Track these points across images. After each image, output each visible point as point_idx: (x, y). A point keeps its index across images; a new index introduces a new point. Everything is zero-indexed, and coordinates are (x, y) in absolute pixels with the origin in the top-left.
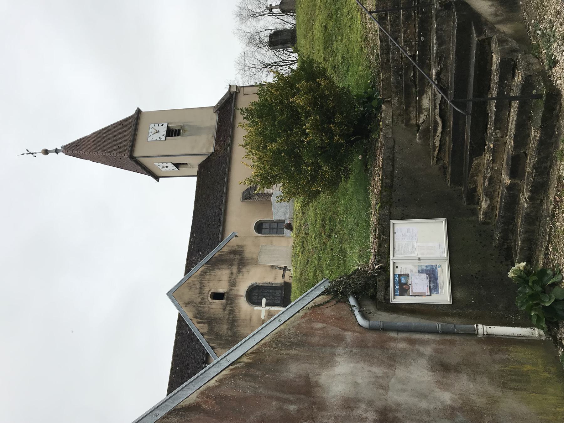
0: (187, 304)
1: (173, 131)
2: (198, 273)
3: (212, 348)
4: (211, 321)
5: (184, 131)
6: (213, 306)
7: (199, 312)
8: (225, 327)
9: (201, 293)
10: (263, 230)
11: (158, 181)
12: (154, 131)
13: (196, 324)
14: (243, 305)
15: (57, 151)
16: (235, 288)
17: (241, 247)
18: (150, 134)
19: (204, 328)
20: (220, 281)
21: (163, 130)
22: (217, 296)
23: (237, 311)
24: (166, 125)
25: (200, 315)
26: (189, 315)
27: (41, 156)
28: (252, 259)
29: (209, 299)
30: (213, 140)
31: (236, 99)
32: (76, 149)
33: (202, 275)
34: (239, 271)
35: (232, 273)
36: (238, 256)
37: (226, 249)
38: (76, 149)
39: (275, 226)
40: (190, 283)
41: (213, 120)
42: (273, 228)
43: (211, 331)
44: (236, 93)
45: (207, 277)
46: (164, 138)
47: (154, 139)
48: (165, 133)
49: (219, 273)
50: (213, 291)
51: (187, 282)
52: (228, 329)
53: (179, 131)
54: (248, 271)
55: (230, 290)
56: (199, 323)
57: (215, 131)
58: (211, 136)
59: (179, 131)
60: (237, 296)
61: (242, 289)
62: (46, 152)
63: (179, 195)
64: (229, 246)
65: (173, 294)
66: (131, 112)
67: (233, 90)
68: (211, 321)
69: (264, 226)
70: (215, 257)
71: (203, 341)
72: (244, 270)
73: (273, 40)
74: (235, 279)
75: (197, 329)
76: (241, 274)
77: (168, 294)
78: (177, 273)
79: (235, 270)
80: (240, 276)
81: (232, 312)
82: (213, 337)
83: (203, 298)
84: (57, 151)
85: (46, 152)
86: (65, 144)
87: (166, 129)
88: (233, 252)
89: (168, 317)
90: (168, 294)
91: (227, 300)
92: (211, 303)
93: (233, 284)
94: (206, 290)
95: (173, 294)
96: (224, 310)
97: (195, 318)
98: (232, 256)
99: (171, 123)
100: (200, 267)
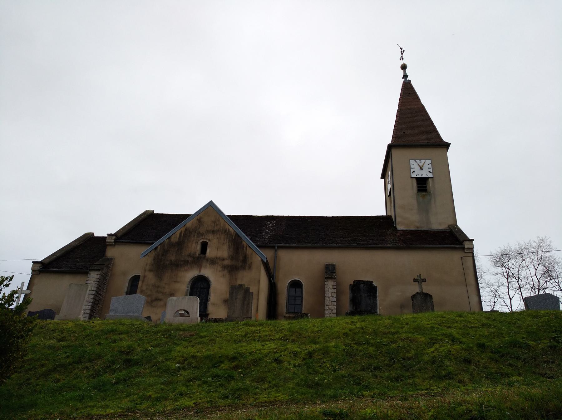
0: (199, 221)
1: (425, 184)
2: (227, 227)
3: (156, 248)
4: (180, 244)
5: (424, 196)
6: (194, 245)
7: (190, 233)
8: (173, 258)
9: (208, 232)
10: (294, 289)
11: (381, 178)
12: (421, 164)
13: (180, 231)
14: (190, 274)
15: (405, 76)
16: (208, 265)
17: (250, 267)
18: (418, 161)
19: (175, 239)
20: (218, 249)
21: (425, 173)
22: (204, 246)
23: (186, 268)
24: (430, 175)
25: (188, 233)
26: (189, 224)
27: (401, 63)
28: (236, 279)
29: (201, 241)
30: (412, 228)
31: (455, 249)
32: (408, 93)
33: (226, 231)
34: (225, 267)
35: (223, 260)
36: (240, 264)
37: (249, 251)
38: (408, 93)
39: (298, 302)
40: (219, 220)
41: (438, 224)
42: (295, 299)
43: (171, 245)
44: (463, 248)
45: (223, 236)
46: (414, 175)
47: (412, 166)
48: (420, 176)
49: (226, 247)
50: (209, 243)
51: (221, 219)
52: (171, 261)
53: (426, 190)
54: (223, 276)
55: (207, 260)
56: (181, 233)
57: (425, 228)
58: (418, 225)
59: (426, 190)
60: (200, 267)
61: (207, 272)
62: (404, 67)
63: (368, 200)
64: (252, 254)
65: (211, 207)
66: (445, 139)
67: (467, 245)
68: (180, 244)
69: (297, 289)
70: (241, 242)
71: (164, 239)
72: (226, 271)
73: (362, 286)
74: (218, 263)
75: (175, 233)
76: (221, 269)
77: (211, 202)
78: (230, 207)
79: (226, 262)
80: (219, 268)
81: (186, 263)
82: (166, 247)
83: (202, 234)
84: (405, 76)
85: (404, 67)
86: (412, 82)
87: (425, 176)
88: (245, 259)
89: (188, 205)
90: (211, 202)
91: (198, 258)
92: (197, 242)
93: (213, 262)
94: (210, 237)
95: (211, 207)
96: (189, 256)
97: (186, 230)
98: (241, 258)
99: (433, 181)
100: (233, 228)
